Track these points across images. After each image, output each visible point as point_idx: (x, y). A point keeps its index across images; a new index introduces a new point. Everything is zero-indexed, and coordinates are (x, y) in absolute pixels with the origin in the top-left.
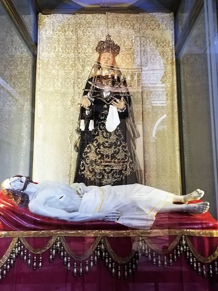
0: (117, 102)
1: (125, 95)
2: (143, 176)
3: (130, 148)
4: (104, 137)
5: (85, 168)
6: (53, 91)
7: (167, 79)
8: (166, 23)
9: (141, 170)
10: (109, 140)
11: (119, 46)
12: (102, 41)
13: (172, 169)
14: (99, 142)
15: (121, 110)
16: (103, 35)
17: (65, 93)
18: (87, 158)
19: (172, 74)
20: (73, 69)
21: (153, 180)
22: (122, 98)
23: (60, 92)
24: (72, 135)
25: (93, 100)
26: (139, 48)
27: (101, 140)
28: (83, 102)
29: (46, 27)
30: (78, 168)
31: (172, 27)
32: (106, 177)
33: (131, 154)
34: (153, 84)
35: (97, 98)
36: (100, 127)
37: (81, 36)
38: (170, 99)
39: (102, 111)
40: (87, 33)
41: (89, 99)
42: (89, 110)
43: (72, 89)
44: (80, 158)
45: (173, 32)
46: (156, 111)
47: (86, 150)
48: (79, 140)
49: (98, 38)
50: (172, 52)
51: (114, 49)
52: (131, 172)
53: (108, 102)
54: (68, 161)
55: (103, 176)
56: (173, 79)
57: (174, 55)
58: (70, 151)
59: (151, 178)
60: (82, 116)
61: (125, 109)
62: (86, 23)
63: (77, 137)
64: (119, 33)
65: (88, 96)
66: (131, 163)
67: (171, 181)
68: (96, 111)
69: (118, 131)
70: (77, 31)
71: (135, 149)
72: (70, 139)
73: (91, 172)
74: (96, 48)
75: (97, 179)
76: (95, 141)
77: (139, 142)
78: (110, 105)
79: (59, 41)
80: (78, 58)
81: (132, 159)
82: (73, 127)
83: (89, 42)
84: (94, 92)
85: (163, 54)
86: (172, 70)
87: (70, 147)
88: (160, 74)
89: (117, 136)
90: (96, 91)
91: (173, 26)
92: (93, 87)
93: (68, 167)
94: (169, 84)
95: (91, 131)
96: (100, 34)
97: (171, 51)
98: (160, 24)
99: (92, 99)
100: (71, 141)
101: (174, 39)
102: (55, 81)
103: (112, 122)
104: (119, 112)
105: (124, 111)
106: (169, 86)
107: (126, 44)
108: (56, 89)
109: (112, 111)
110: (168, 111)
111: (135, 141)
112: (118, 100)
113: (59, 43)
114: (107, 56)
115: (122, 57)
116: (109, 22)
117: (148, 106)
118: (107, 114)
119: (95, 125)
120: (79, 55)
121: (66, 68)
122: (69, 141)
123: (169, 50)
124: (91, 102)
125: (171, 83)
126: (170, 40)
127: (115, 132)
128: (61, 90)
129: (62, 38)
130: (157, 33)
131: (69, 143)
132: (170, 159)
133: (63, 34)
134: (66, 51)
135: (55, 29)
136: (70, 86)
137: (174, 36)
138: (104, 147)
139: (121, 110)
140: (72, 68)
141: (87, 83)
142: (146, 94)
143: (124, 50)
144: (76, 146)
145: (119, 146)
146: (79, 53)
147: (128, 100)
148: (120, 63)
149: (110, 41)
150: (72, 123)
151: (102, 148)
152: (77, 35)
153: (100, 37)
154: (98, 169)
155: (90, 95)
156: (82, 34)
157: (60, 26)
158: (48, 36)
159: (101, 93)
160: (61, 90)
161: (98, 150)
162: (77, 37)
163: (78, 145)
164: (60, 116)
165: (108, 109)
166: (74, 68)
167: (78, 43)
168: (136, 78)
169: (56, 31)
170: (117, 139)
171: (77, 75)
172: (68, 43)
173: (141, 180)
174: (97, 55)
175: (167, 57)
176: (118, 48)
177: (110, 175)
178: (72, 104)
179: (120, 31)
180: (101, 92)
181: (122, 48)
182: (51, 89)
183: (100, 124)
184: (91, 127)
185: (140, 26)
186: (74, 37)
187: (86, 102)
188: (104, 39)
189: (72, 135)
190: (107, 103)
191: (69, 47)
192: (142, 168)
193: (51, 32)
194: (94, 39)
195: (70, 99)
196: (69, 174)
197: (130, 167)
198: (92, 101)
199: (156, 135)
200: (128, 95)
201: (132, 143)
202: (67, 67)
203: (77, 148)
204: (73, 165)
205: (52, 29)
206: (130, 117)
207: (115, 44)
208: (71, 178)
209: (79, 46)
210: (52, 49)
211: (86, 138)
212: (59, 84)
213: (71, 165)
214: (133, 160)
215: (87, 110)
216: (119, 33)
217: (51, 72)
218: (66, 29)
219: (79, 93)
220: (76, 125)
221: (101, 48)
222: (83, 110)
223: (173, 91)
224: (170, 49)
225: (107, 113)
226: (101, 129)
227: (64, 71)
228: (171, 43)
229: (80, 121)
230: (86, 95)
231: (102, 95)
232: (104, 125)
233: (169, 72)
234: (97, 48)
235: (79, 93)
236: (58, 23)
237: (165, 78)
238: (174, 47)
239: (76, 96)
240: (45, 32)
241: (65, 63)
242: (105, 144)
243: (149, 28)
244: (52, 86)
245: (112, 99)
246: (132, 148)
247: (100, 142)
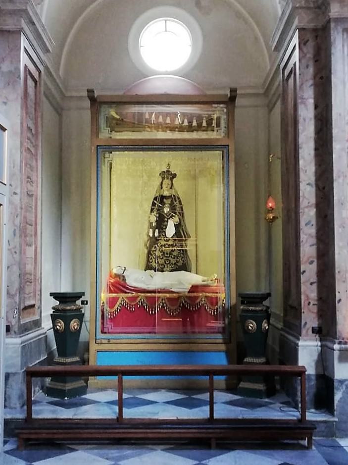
25: (158, 215)
27: (163, 243)
30: (148, 261)
52: (182, 263)
55: (164, 267)
103: (170, 231)
104: (174, 224)
118: (167, 225)
154: (161, 261)
165: (167, 221)
184: (157, 234)
187: (153, 218)
211: (154, 241)
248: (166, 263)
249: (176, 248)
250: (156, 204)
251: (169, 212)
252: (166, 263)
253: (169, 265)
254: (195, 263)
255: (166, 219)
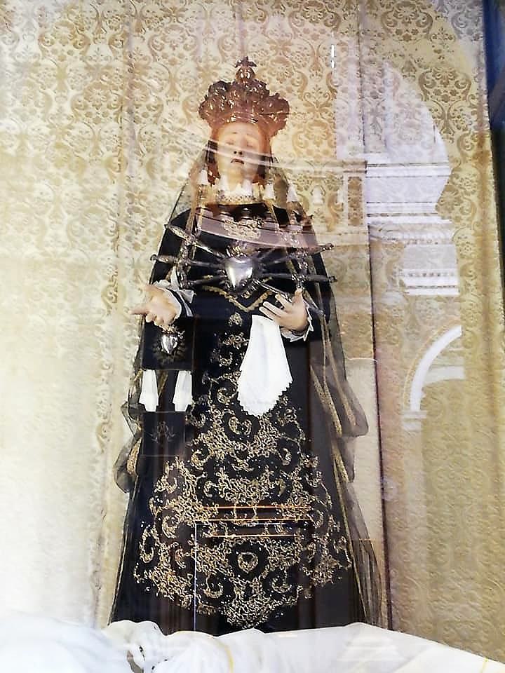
0: (279, 305)
1: (310, 278)
2: (383, 581)
3: (329, 477)
4: (231, 436)
5: (156, 558)
6: (40, 258)
7: (464, 214)
8: (453, 13)
9: (368, 545)
10: (249, 446)
11: (283, 101)
12: (221, 83)
13: (490, 552)
14: (212, 454)
15: (295, 332)
16: (224, 55)
17: (81, 263)
18: (167, 518)
19: (483, 197)
20: (112, 176)
21: (417, 595)
22: (299, 290)
23: (64, 262)
24: (106, 421)
25: (190, 295)
26: (354, 104)
27: (220, 447)
28: (154, 305)
29: (17, 29)
30: (130, 557)
31: (478, 29)
32: (239, 593)
33: (335, 499)
34: (432, 287)
35: (206, 288)
36: (214, 397)
37: (145, 59)
38: (477, 286)
39: (224, 338)
40: (168, 50)
41: (175, 294)
42: (176, 335)
43: (110, 251)
44: (140, 516)
45: (480, 45)
46: (419, 321)
47: (163, 485)
48: (137, 447)
49: (207, 67)
50: (480, 116)
51: (267, 108)
52: (337, 572)
53: (247, 303)
54: (89, 524)
55: (229, 588)
56: (484, 215)
57: (487, 127)
58: (98, 485)
59: (413, 589)
60: (149, 356)
61: (311, 328)
62: (160, 13)
63: (125, 433)
64: (285, 49)
65: (170, 281)
66: (336, 535)
67: (490, 602)
68: (203, 341)
69: (283, 411)
70: (129, 43)
71: (352, 478)
72: (98, 438)
73: (179, 573)
74: (202, 105)
75: (205, 598)
76: (198, 452)
77: (364, 450)
78: (254, 317)
79: (61, 76)
80: (133, 137)
81: (339, 518)
82: (112, 391)
83: (172, 80)
84: (194, 268)
85: (446, 122)
86: (482, 180)
87: (98, 467)
88: (434, 177)
89: (281, 430)
90: (200, 263)
91: (481, 23)
92: (190, 247)
93: (93, 545)
94: (473, 232)
95: (181, 414)
96: (214, 52)
97: (473, 113)
98: (434, 19)
99: (185, 292)
100: (102, 445)
101: (484, 71)
102: (47, 221)
103: (263, 377)
104: (286, 342)
105: (305, 338)
106: (471, 239)
107: (309, 89)
108: (49, 249)
109: (262, 336)
110: (472, 332)
111: (349, 448)
112: (281, 298)
113: (64, 83)
114: (238, 136)
115: (296, 135)
116: (245, 10)
117: (392, 298)
118: (244, 349)
119: (198, 390)
120: (137, 127)
121: (87, 175)
122: (96, 445)
123: (468, 111)
124: (183, 306)
125: (479, 230)
126: (472, 74)
127: (274, 415)
128: (68, 255)
129: (75, 64)
130: (424, 50)
131: (93, 451)
132: (485, 515)
133: (77, 52)
134: (89, 115)
135: (49, 35)
136: (102, 241)
137: (483, 61)
138: (232, 474)
139: (295, 332)
140: (110, 173)
141: (169, 236)
142: (387, 270)
143: (303, 109)
144: (123, 468)
145: (289, 469)
146: (136, 120)
147: (321, 291)
148: (290, 155)
149: (252, 82)
150: (108, 375)
151: (223, 476)
152: (131, 56)
153: (212, 63)
154: (208, 560)
155: (179, 278)
156: (147, 53)
157: (66, 24)
158: (21, 60)
159: (218, 269)
160: (68, 255)
161: (210, 484)
162: (131, 65)
163: (131, 466)
164: (61, 351)
165: (245, 329)
166: (116, 174)
167: (132, 86)
168: (343, 196)
169: (53, 43)
170: (281, 444)
171: (128, 200)
172: (99, 86)
173: (377, 611)
174: (201, 131)
175: (459, 133)
176: (281, 105)
177: (256, 583)
178: (109, 307)
179: (286, 44)
180: (218, 266)
181: (294, 102)
182: (31, 251)
183: (216, 387)
184: (183, 398)
185: (358, 25)
186: (119, 64)
187: (165, 307)
188: (228, 73)
189: (107, 423)
190: (241, 307)
191: (99, 97)
192: (373, 532)
193: (35, 47)
194: (193, 72)
195: (101, 288)
196: (95, 572)
197: (332, 551)
198: (186, 301)
199: (422, 408)
200: (322, 278)
201: (338, 458)
202: (90, 169)
203: (129, 477)
204: (109, 537)
205: (37, 35)
206: (328, 363)
207: (271, 94)
208: (103, 590)
209: (137, 93)
210: (37, 105)
211: (160, 436)
212: (62, 232)
213: (100, 540)
214: (343, 523)
215: (166, 333)
216: (285, 49)
217: (30, 189)
218: (89, 34)
219: (136, 266)
220: (127, 388)
221: (217, 109)
222: (150, 332)
223: (484, 255)
224: (472, 106)
225: (242, 344)
226: (221, 407)
227: (80, 185)
228: (475, 86)
229: (141, 376)
230: (164, 278)
231: (223, 279)
232: (232, 389)
233: (469, 189)
234: (203, 107)
235: (136, 266)
236: (91, 78)
237: (457, 208)
238: (485, 97)
239: (125, 276)
240: (11, 47)
241: (85, 156)
242: (236, 463)
243: (394, 30)
244: (33, 238)
245: (261, 291)
246: (340, 476)
247: (214, 457)
248: (237, 571)
249: (175, 133)
250: (180, 240)
251: (249, 281)
252: (237, 571)
253: (256, 583)
254: (376, 413)
255: (236, 319)
